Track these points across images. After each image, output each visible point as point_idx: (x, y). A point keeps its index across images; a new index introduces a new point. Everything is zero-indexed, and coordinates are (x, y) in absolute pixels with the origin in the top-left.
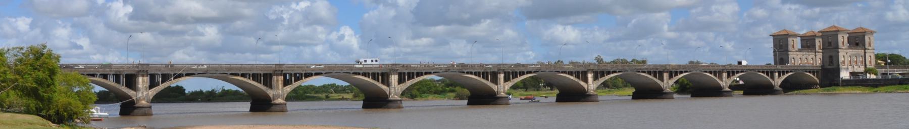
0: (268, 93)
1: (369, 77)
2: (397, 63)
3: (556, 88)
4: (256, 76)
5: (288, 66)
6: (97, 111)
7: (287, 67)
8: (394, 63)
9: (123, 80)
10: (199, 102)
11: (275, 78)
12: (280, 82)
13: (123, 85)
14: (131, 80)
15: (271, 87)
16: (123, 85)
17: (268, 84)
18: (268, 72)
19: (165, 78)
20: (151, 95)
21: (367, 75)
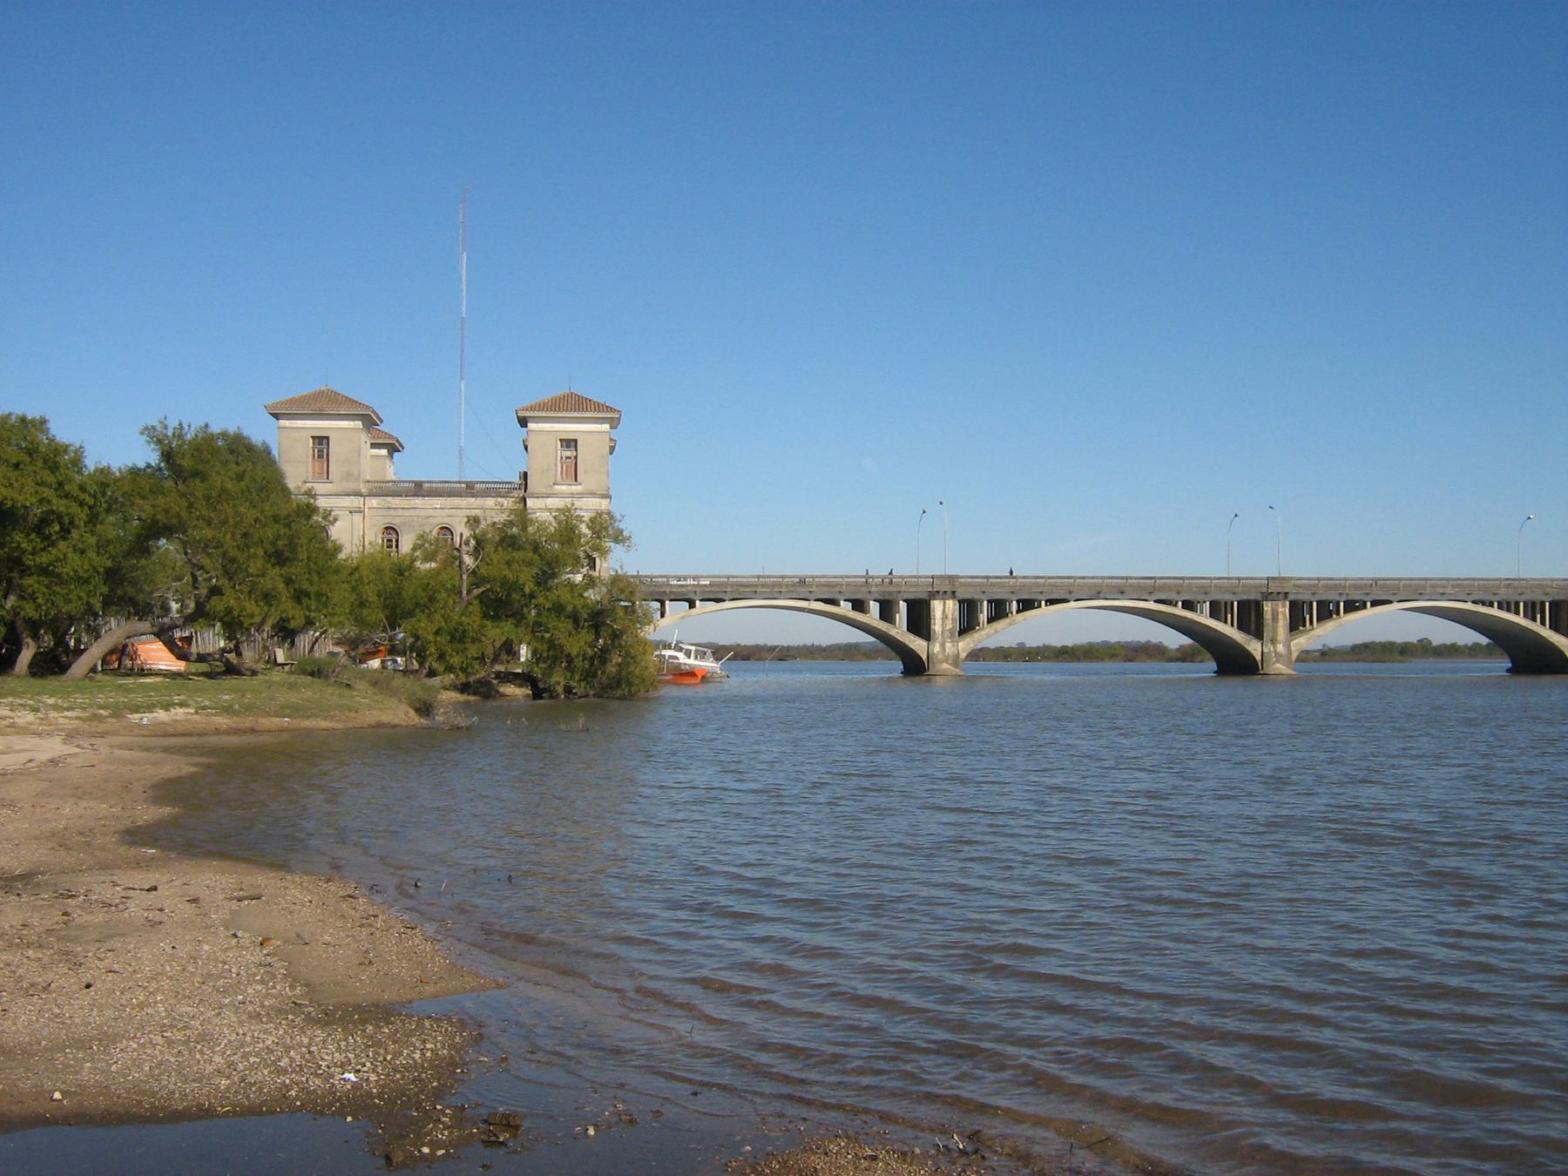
0: (1249, 649)
1: (1517, 613)
2: (1282, 575)
3: (1208, 655)
4: (1253, 605)
5: (1299, 582)
6: (511, 690)
7: (1295, 586)
8: (1276, 575)
9: (874, 607)
10: (1039, 661)
11: (1267, 607)
12: (1281, 623)
13: (1232, 625)
14: (1250, 616)
15: (1258, 634)
16: (1232, 625)
17: (1253, 627)
18: (1252, 597)
19: (999, 611)
20: (963, 650)
21: (1505, 606)
